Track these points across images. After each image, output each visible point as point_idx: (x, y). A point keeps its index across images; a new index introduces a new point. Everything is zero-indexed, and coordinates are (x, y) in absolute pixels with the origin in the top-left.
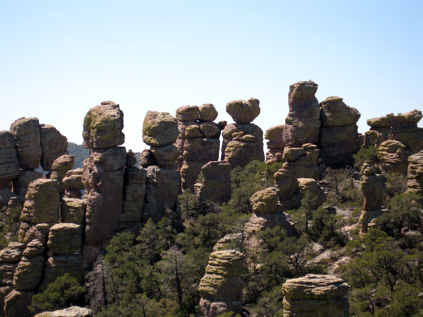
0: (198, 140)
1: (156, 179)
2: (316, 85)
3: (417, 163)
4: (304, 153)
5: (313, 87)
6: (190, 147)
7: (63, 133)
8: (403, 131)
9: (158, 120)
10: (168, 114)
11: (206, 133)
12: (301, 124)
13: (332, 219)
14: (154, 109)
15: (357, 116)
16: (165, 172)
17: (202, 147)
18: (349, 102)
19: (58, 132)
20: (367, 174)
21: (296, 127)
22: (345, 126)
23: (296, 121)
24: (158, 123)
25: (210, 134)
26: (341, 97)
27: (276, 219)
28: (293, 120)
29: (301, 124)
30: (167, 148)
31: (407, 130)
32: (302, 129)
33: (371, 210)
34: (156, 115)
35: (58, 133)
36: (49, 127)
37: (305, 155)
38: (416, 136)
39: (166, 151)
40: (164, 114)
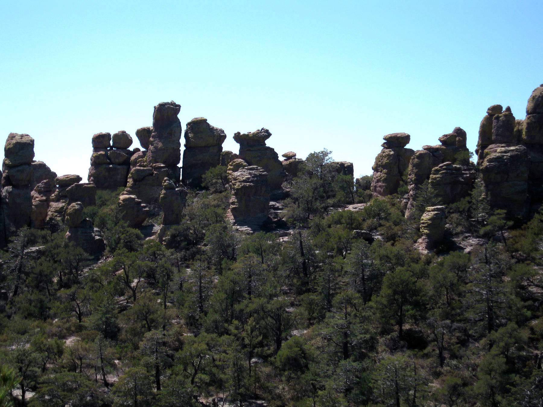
0: (104, 166)
1: (8, 199)
2: (179, 106)
3: (237, 180)
4: (151, 172)
5: (406, 139)
6: (95, 173)
7: (53, 170)
8: (248, 150)
9: (14, 141)
10: (28, 135)
11: (112, 160)
12: (160, 145)
13: (127, 232)
14: (14, 132)
15: (221, 137)
16: (17, 191)
17: (107, 174)
18: (214, 123)
19: (48, 168)
20: (166, 188)
21: (156, 148)
22: (207, 147)
23: (156, 142)
24: (14, 144)
25: (117, 161)
26: (205, 118)
27: (79, 233)
28: (154, 141)
29: (160, 145)
30: (19, 168)
31: (251, 149)
32: (161, 149)
33: (168, 224)
34: (15, 137)
35: (47, 170)
36: (39, 163)
37: (152, 174)
38: (260, 154)
39: (18, 171)
40: (22, 136)
